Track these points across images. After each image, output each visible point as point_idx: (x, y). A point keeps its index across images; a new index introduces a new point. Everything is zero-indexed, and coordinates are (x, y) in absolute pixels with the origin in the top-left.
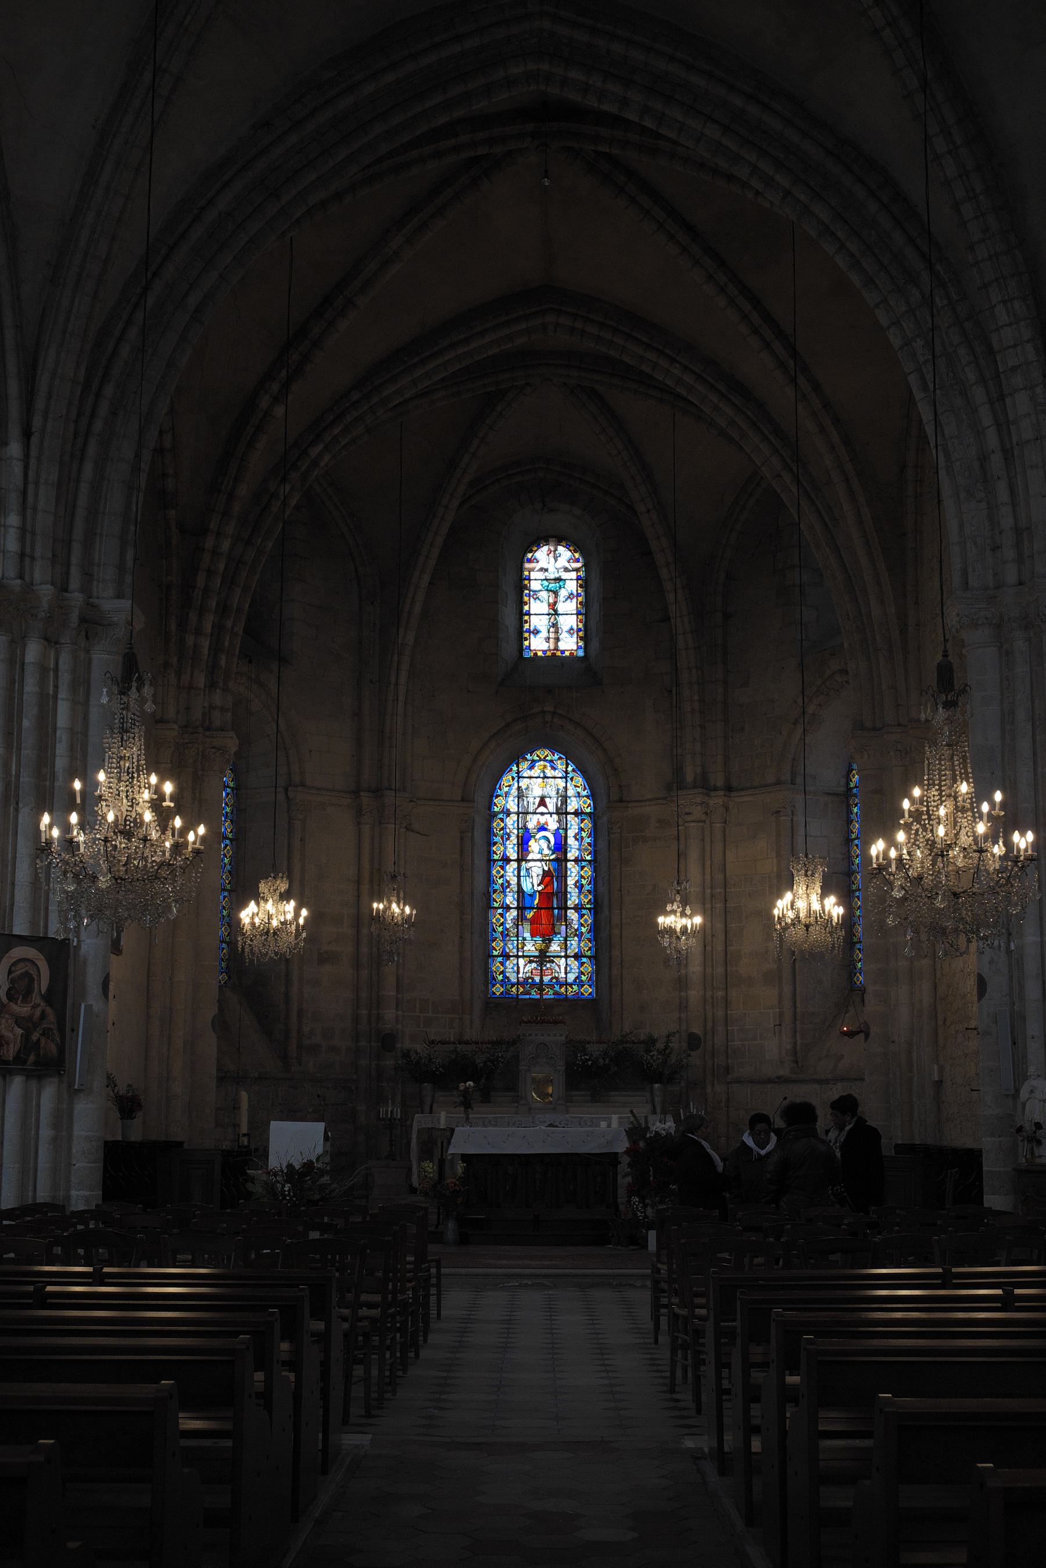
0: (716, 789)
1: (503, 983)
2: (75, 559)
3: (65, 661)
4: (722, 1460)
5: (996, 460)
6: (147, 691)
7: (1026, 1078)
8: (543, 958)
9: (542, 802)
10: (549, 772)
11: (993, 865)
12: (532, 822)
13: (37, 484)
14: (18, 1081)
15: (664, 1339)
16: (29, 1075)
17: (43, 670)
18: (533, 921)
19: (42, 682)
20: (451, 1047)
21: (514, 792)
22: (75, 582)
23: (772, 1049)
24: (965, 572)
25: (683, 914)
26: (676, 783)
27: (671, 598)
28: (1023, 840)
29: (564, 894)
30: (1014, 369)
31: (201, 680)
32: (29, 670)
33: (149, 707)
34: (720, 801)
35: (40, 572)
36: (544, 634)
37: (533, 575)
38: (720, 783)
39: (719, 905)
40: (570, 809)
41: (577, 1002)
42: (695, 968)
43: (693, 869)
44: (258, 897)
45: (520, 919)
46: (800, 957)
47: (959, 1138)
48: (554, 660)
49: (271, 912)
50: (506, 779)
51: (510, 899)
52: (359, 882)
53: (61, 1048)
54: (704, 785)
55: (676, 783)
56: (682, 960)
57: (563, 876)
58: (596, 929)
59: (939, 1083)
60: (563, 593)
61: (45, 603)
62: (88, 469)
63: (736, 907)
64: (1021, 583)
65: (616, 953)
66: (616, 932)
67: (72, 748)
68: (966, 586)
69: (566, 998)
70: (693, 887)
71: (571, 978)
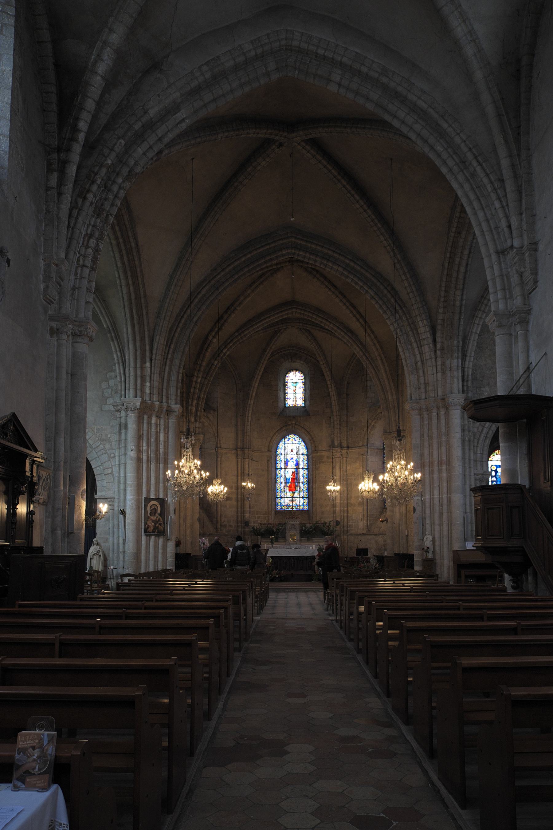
0: (344, 447)
1: (280, 506)
2: (164, 394)
3: (162, 422)
4: (337, 621)
5: (420, 364)
6: (193, 438)
7: (426, 535)
8: (293, 499)
9: (292, 451)
10: (294, 442)
11: (410, 481)
12: (289, 457)
13: (154, 373)
14: (153, 537)
15: (326, 602)
16: (156, 536)
17: (156, 425)
18: (289, 487)
19: (156, 428)
20: (266, 525)
21: (283, 448)
22: (164, 400)
23: (361, 525)
24: (411, 394)
25: (334, 486)
26: (332, 446)
27: (330, 390)
28: (418, 476)
29: (298, 479)
30: (424, 339)
31: (193, 419)
32: (153, 425)
33: (193, 442)
34: (345, 451)
35: (155, 398)
36: (292, 399)
37: (288, 381)
38: (345, 446)
39: (345, 482)
40: (300, 453)
41: (303, 511)
42: (338, 501)
43: (337, 472)
44: (212, 484)
45: (286, 486)
46: (366, 501)
47: (412, 551)
48: (295, 408)
49: (217, 489)
50: (281, 444)
51: (283, 480)
52: (237, 476)
53: (164, 528)
54: (341, 446)
55: (332, 446)
56: (334, 499)
57: (298, 473)
58: (308, 489)
59: (407, 535)
60: (298, 387)
61: (157, 407)
62: (167, 368)
63: (349, 484)
64: (426, 399)
65: (314, 497)
66: (314, 490)
67: (164, 446)
68: (411, 399)
69: (300, 510)
70: (337, 478)
71: (301, 504)
